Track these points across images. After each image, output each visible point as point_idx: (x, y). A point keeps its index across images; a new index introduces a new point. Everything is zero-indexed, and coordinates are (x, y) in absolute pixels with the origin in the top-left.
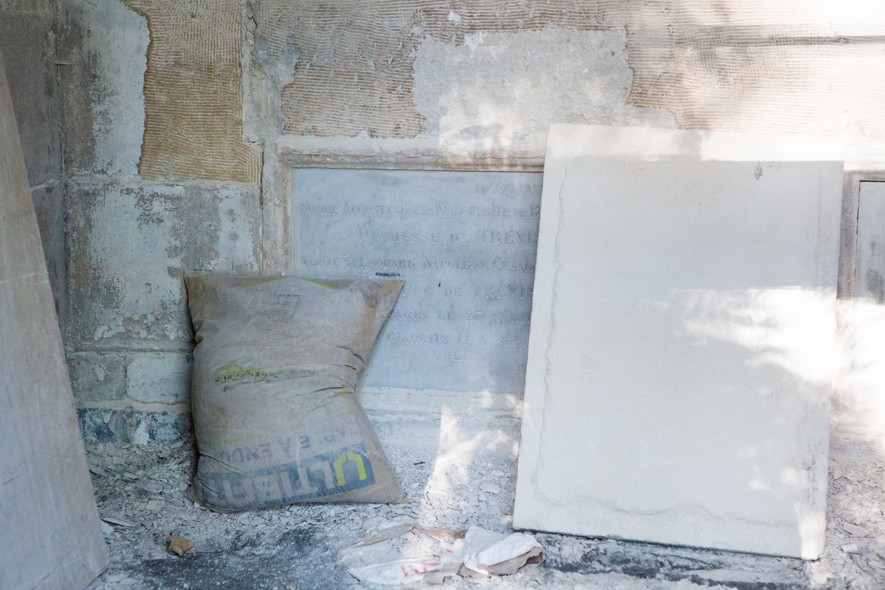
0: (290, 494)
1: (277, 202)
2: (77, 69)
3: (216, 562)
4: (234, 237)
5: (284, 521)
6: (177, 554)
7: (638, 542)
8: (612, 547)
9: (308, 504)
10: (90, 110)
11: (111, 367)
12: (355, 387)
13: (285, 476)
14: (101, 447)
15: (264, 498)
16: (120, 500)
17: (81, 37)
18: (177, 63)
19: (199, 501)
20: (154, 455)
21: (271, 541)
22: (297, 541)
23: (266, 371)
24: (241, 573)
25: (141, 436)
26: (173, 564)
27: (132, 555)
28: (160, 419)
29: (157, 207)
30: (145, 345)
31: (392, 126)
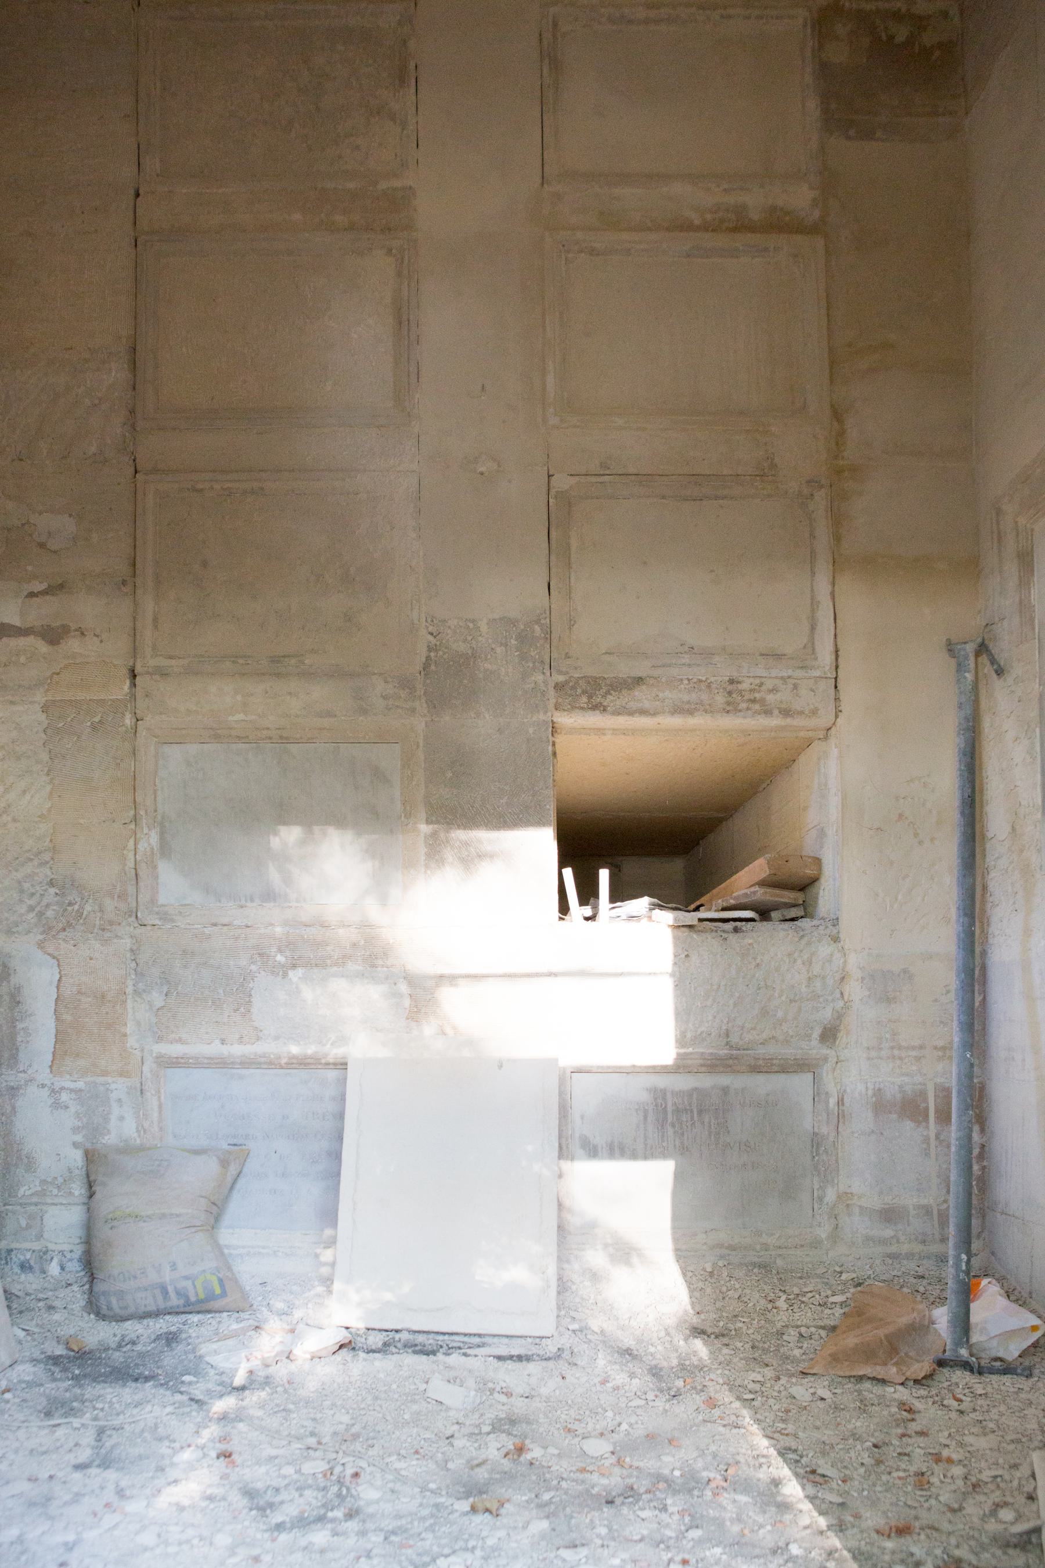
0: (162, 1305)
1: (154, 1092)
2: (6, 998)
3: (104, 1355)
4: (121, 1118)
5: (158, 1326)
6: (73, 1351)
7: (424, 1332)
8: (404, 1336)
9: (177, 1313)
10: (15, 1027)
11: (31, 1217)
12: (213, 1228)
13: (158, 1293)
14: (23, 1276)
15: (142, 1309)
16: (33, 1313)
17: (9, 975)
18: (79, 992)
19: (95, 1314)
20: (64, 1282)
21: (148, 1340)
22: (167, 1340)
23: (143, 1214)
24: (123, 1362)
25: (54, 1269)
26: (69, 1358)
27: (39, 1352)
28: (68, 1255)
29: (64, 1097)
30: (56, 1201)
31: (237, 1036)
